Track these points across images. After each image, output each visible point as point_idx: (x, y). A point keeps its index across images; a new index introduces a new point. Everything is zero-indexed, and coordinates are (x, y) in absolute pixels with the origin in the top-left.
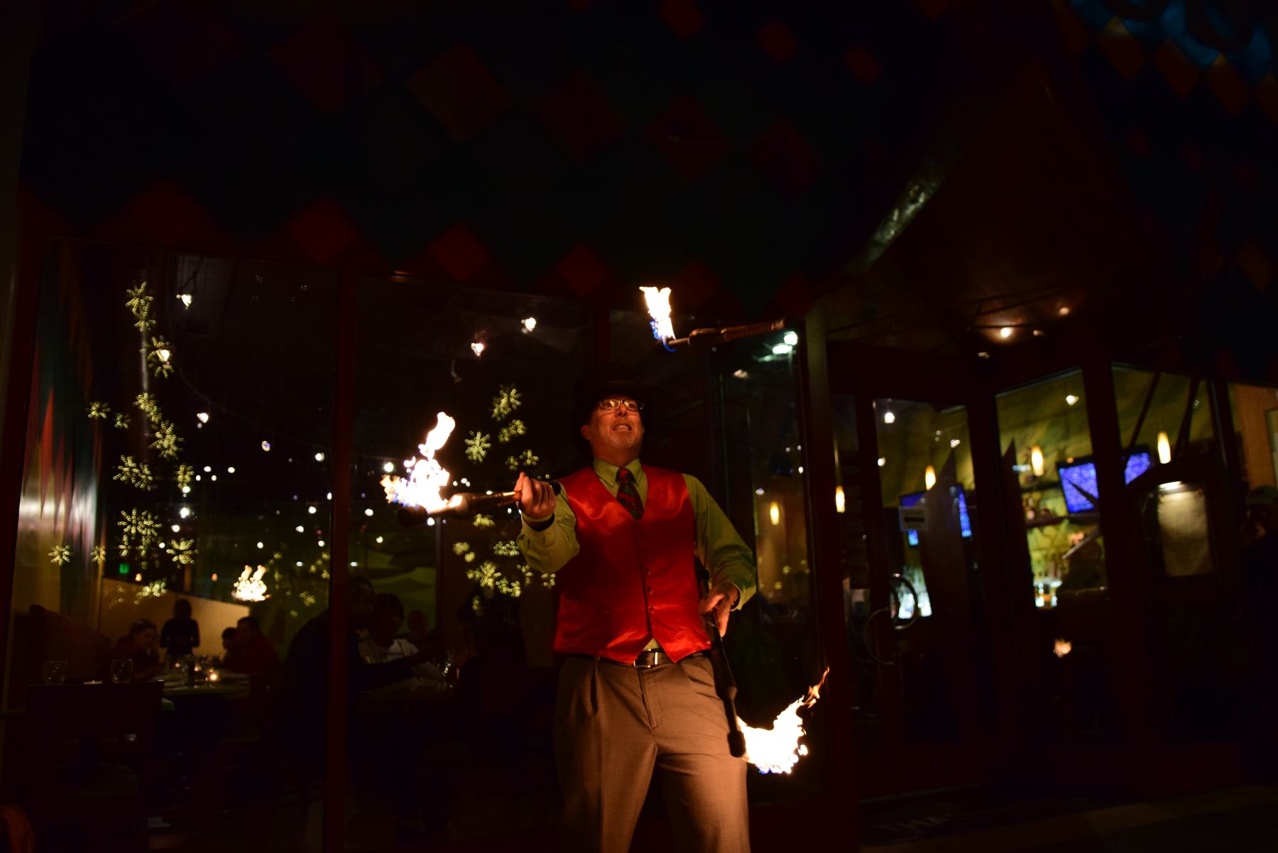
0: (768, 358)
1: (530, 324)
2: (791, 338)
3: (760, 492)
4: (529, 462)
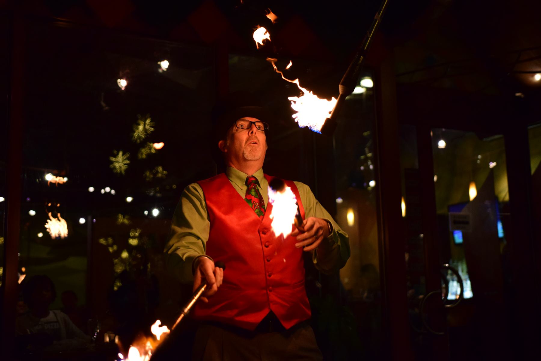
1: (165, 65)
4: (160, 175)
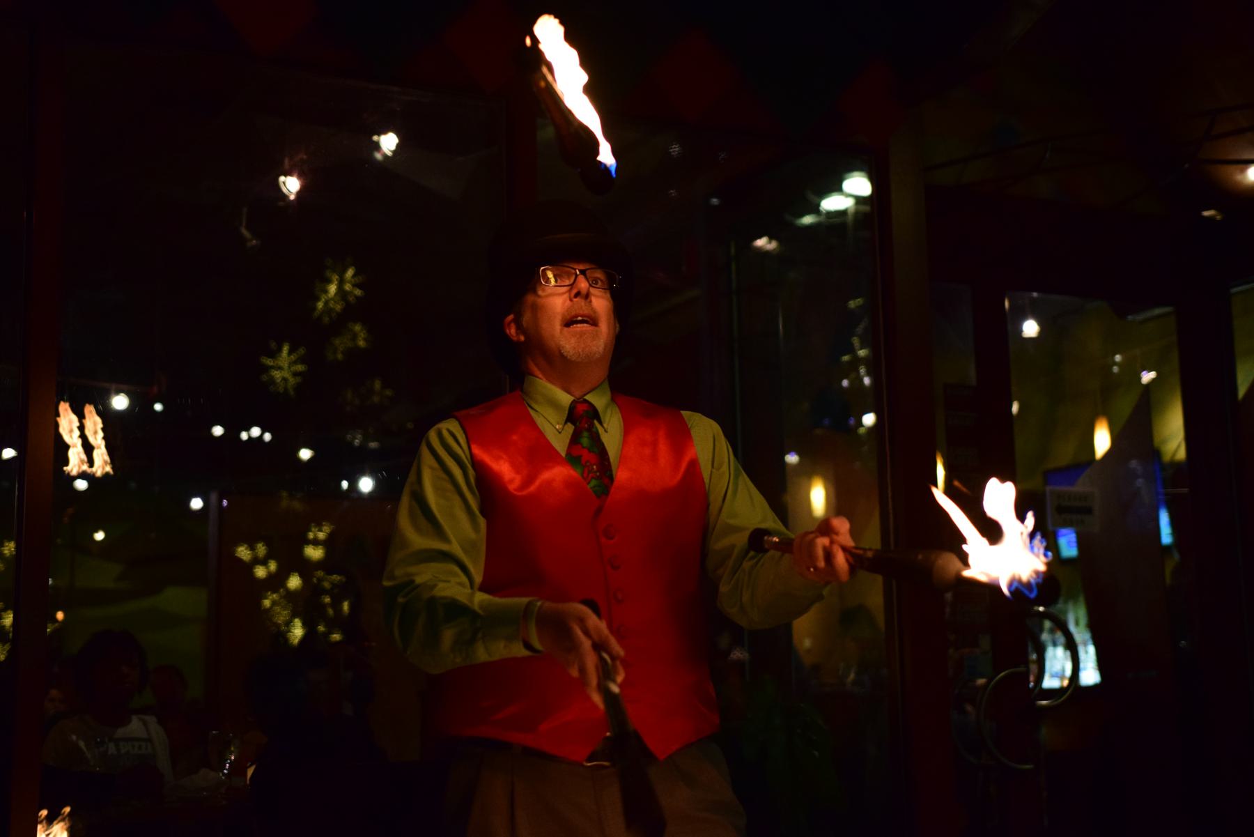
0: (808, 220)
1: (389, 142)
2: (858, 185)
3: (792, 459)
4: (376, 399)
